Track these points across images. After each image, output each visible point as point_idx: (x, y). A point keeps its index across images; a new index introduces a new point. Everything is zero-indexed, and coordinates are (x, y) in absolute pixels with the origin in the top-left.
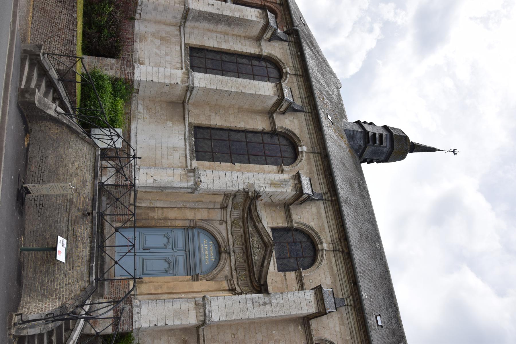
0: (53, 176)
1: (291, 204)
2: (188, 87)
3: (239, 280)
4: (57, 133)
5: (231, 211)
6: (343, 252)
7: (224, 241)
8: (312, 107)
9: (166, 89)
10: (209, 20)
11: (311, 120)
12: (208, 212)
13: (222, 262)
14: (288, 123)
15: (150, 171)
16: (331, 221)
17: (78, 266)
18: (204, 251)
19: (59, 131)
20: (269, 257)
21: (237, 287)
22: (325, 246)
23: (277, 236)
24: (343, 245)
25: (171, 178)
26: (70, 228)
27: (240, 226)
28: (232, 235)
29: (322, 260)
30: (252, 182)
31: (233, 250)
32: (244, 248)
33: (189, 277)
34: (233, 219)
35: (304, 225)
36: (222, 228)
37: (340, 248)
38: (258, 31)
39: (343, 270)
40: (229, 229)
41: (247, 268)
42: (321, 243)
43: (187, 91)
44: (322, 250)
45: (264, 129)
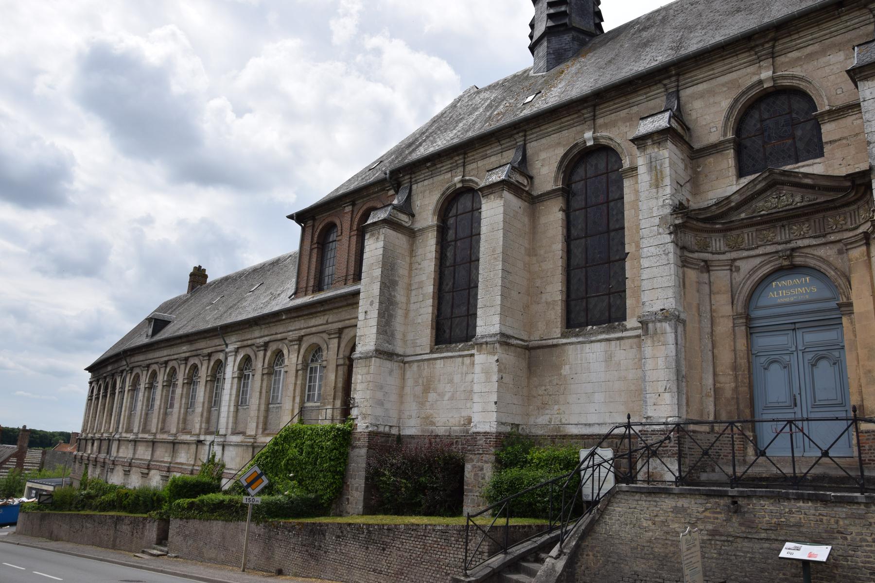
0: (669, 564)
1: (691, 148)
2: (502, 343)
3: (845, 227)
4: (594, 555)
5: (713, 253)
6: (775, 40)
7: (771, 262)
8: (515, 132)
9: (507, 379)
10: (391, 316)
11: (538, 129)
12: (718, 293)
13: (812, 262)
14: (546, 169)
15: (651, 398)
16: (716, 71)
17: (837, 522)
18: (790, 296)
19: (590, 553)
20: (795, 177)
21: (860, 230)
22: (766, 74)
23: (754, 165)
24: (762, 41)
25: (661, 362)
26: (763, 535)
27: (738, 235)
28: (757, 248)
29: (793, 77)
30: (657, 221)
31: (786, 243)
32: (780, 224)
33: (845, 320)
34: (727, 249)
35: (727, 118)
36: (745, 266)
37: (767, 46)
38: (400, 235)
39: (812, 34)
40: (745, 254)
41: (821, 215)
42: (760, 82)
43: (508, 344)
44: (773, 79)
45: (561, 210)
